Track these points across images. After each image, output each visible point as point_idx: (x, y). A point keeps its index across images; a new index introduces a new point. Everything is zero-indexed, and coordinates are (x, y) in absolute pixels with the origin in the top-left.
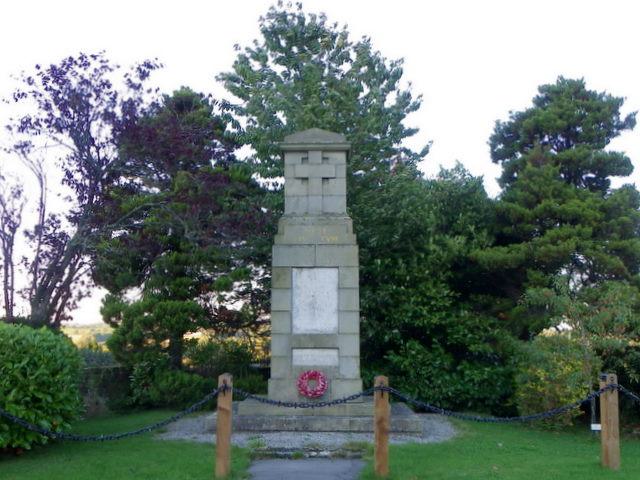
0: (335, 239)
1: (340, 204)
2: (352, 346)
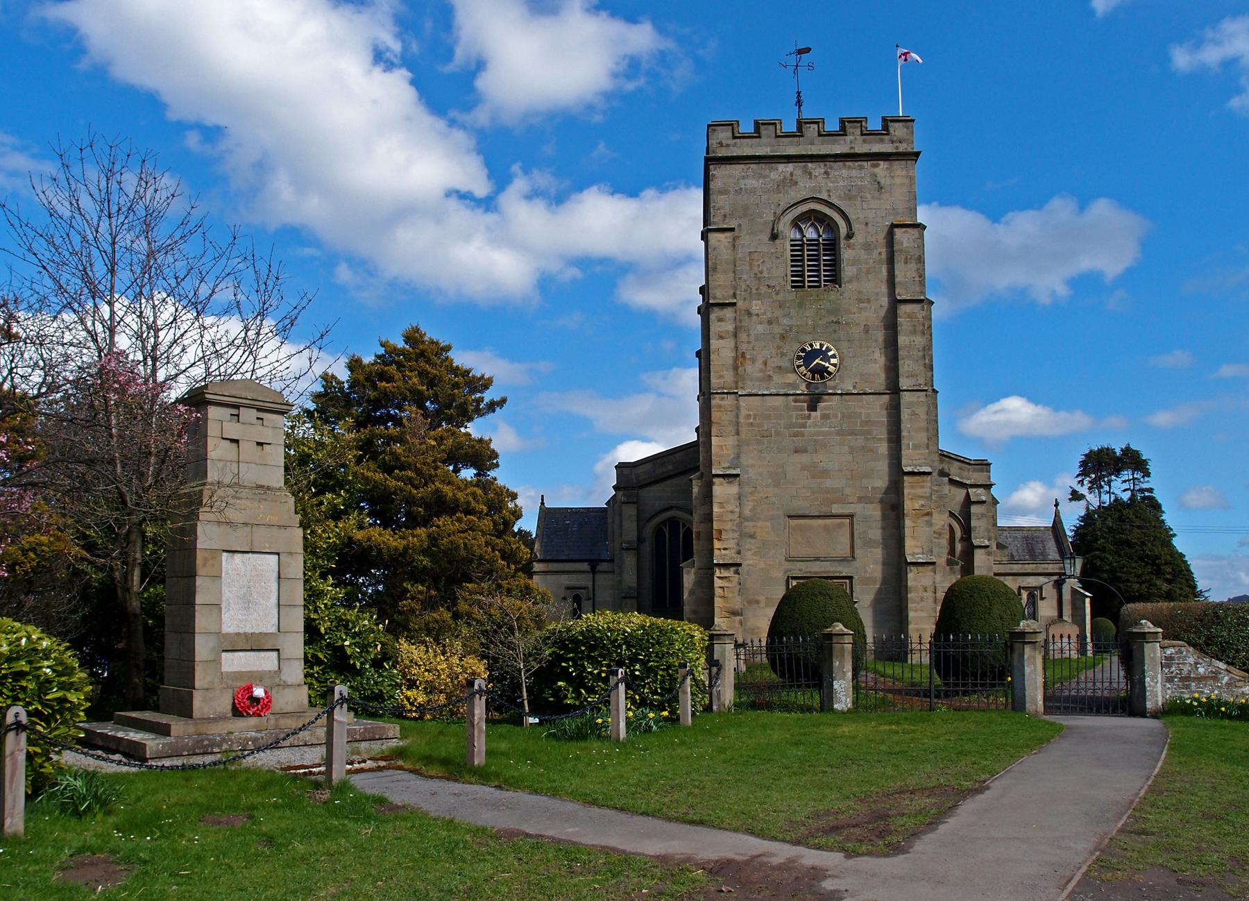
0: (275, 519)
1: (277, 478)
2: (295, 645)
